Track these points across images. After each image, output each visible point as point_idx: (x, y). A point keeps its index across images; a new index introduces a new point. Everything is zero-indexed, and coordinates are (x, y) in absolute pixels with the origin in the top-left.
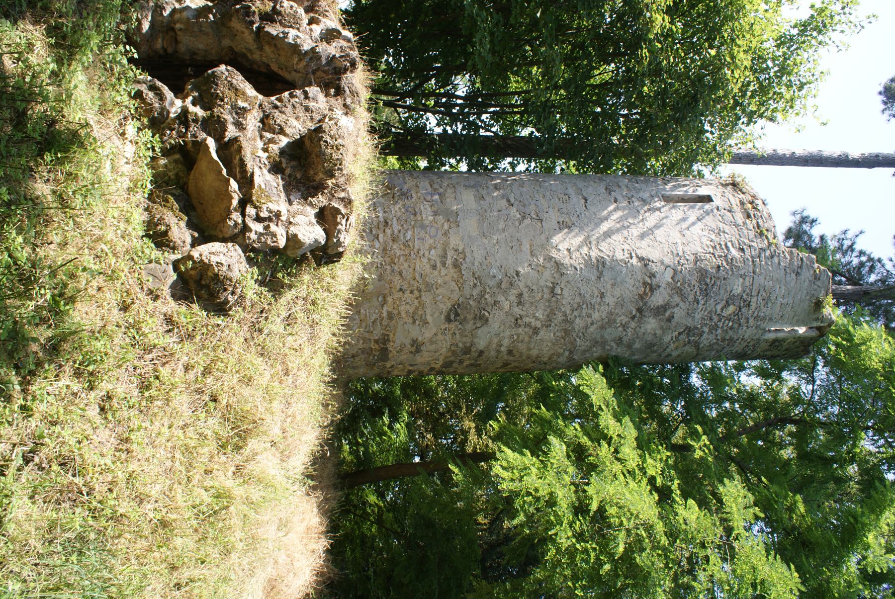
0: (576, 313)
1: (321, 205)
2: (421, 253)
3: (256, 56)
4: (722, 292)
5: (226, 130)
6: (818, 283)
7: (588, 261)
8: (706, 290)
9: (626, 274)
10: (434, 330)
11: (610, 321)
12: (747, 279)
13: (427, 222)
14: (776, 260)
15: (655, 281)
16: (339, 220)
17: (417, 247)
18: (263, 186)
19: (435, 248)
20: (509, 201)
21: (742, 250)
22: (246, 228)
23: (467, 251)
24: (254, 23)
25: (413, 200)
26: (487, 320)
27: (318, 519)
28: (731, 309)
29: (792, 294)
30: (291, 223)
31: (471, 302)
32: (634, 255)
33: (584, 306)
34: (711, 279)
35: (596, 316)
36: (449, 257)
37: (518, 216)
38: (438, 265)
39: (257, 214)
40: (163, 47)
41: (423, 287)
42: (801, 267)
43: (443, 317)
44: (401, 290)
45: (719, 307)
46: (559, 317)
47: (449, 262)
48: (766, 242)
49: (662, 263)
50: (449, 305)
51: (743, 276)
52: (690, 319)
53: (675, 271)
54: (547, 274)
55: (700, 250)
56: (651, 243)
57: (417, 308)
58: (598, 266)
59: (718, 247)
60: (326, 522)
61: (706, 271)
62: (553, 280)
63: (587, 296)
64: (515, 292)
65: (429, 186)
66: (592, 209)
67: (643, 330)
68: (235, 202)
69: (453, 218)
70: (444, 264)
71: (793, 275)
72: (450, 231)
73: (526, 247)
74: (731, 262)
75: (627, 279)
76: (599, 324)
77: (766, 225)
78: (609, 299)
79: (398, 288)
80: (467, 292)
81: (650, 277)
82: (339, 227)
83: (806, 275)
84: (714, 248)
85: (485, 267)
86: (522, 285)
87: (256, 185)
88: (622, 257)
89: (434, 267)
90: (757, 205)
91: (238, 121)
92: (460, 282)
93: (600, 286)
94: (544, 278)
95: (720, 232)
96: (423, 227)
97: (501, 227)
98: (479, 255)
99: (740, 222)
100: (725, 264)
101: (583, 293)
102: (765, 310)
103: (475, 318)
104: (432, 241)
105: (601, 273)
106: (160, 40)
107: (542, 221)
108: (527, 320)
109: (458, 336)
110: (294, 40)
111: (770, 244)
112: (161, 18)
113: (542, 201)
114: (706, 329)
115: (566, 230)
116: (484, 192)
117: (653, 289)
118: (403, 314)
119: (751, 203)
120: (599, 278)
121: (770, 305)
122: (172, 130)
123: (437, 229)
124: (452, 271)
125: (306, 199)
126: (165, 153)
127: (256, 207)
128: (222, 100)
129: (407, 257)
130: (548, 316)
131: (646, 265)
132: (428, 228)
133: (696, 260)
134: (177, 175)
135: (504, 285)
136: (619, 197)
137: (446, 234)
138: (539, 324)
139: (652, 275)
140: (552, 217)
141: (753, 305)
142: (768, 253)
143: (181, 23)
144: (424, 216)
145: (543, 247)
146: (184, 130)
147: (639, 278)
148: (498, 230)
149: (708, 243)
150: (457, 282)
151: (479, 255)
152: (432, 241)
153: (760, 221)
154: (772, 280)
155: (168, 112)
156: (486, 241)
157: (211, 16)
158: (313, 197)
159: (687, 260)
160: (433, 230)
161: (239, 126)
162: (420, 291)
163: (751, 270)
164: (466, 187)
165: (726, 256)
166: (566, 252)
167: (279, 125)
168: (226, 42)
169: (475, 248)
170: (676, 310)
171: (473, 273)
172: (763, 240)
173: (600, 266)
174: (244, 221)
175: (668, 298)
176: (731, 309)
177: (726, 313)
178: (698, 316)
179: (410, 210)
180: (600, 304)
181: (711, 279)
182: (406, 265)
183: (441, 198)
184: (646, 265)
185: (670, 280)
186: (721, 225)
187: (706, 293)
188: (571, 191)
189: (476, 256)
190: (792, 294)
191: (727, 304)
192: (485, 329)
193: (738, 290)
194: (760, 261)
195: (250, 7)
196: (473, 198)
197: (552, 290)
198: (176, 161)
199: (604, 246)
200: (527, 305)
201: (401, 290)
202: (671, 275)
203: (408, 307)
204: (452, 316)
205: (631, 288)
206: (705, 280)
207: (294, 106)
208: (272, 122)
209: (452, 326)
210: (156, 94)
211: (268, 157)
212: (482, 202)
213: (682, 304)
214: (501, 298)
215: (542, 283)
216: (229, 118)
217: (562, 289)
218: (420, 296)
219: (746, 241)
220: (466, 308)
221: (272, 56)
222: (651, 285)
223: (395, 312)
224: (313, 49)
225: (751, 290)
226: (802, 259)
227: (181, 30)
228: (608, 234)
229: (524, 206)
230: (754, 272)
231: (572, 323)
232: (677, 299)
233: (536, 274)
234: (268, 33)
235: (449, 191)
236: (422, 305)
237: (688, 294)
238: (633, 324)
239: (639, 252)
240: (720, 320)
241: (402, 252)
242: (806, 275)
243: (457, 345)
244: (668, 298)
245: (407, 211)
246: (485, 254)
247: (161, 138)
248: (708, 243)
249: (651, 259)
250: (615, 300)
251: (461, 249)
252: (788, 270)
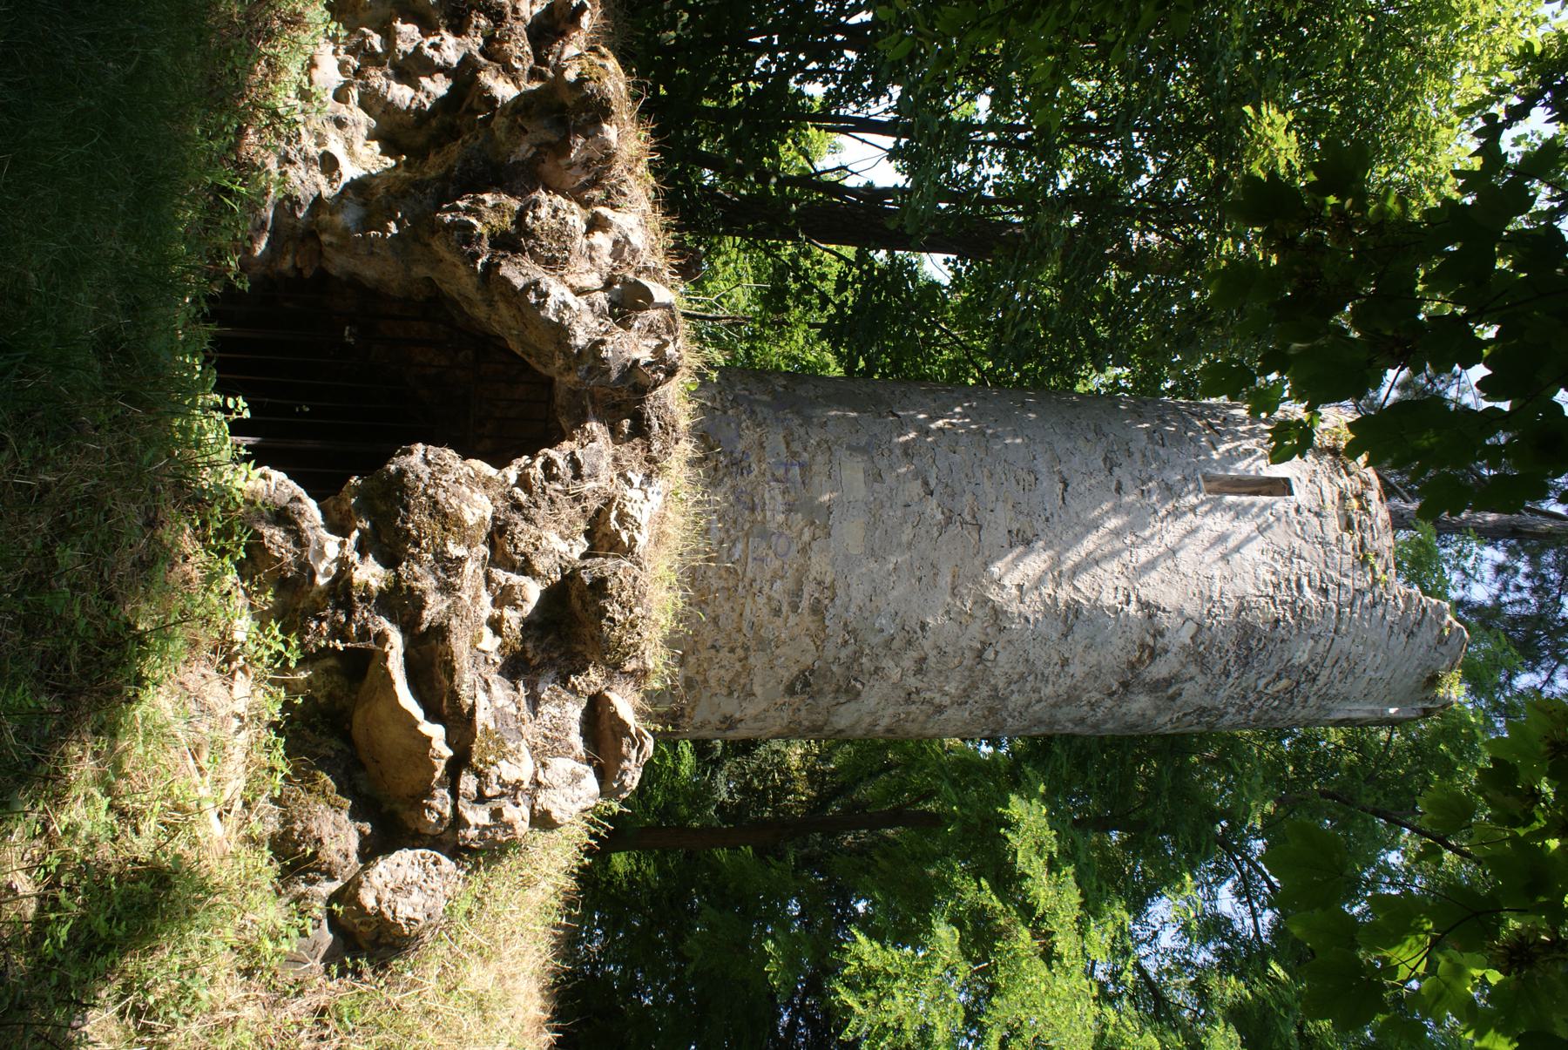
0: (1013, 687)
1: (593, 689)
2: (756, 586)
3: (481, 312)
4: (1273, 660)
5: (423, 608)
6: (1443, 650)
7: (1051, 609)
8: (1246, 657)
9: (1114, 632)
10: (764, 705)
11: (1071, 698)
12: (1322, 641)
13: (772, 526)
14: (1379, 610)
15: (1161, 642)
16: (624, 749)
17: (750, 575)
18: (492, 726)
19: (782, 578)
20: (926, 483)
21: (1325, 592)
22: (458, 821)
23: (840, 584)
24: (479, 257)
25: (752, 476)
26: (858, 694)
27: (539, 1002)
28: (1284, 683)
29: (1393, 666)
30: (539, 784)
31: (835, 668)
32: (1133, 598)
33: (1031, 678)
34: (1259, 640)
35: (1048, 690)
36: (806, 595)
37: (940, 517)
38: (785, 608)
39: (480, 790)
40: (294, 266)
41: (752, 644)
42: (1419, 624)
43: (781, 687)
44: (713, 647)
45: (1262, 683)
46: (985, 691)
47: (805, 604)
48: (1369, 578)
49: (1180, 612)
50: (795, 670)
51: (1316, 638)
52: (1208, 698)
53: (1200, 626)
54: (975, 629)
55: (1252, 591)
56: (1168, 576)
57: (738, 674)
58: (1066, 617)
59: (1283, 586)
60: (550, 1005)
61: (1254, 628)
62: (983, 638)
63: (1040, 664)
64: (915, 654)
65: (783, 446)
66: (1075, 505)
67: (1124, 710)
68: (441, 766)
69: (821, 519)
70: (795, 608)
71: (1403, 637)
72: (814, 545)
73: (945, 580)
74: (1300, 613)
75: (1114, 639)
76: (1051, 701)
77: (1376, 545)
78: (1076, 669)
79: (709, 644)
80: (830, 652)
81: (1154, 636)
82: (626, 764)
83: (1426, 636)
84: (1277, 586)
85: (867, 614)
86: (927, 644)
87: (479, 728)
88: (1112, 602)
89: (777, 612)
90: (1369, 502)
91: (446, 584)
92: (819, 638)
93: (1063, 648)
94: (968, 635)
95: (1293, 555)
96: (765, 535)
97: (905, 538)
98: (859, 593)
99: (1332, 537)
100: (1288, 615)
101: (1031, 657)
102: (1339, 686)
103: (837, 691)
104: (778, 563)
105: (1071, 628)
106: (289, 258)
107: (981, 527)
108: (928, 695)
109: (803, 713)
110: (558, 312)
111: (1375, 582)
112: (291, 221)
113: (987, 484)
114: (1232, 710)
115: (1021, 549)
116: (883, 464)
117: (1154, 654)
118: (713, 682)
119: (1358, 496)
120: (1065, 636)
121: (1350, 679)
122: (321, 619)
123: (790, 541)
124: (808, 620)
125: (564, 681)
126: (306, 660)
127: (479, 774)
128: (417, 544)
129: (730, 592)
130: (965, 690)
131: (1150, 617)
132: (774, 538)
133: (1241, 608)
134: (330, 696)
135: (896, 645)
136: (1127, 483)
137: (804, 551)
138: (946, 701)
139: (1159, 633)
140: (1001, 520)
141: (1322, 680)
142: (1368, 598)
143: (333, 234)
144: (768, 514)
145: (975, 579)
146: (343, 619)
147: (1135, 637)
148: (899, 545)
149: (1268, 577)
150: (814, 637)
151: (859, 593)
152: (778, 563)
153: (1368, 535)
154: (1364, 643)
155: (313, 574)
156: (873, 565)
157: (393, 227)
158: (578, 673)
159: (1225, 608)
160: (782, 541)
161: (446, 589)
162: (747, 649)
163: (1332, 627)
165: (1294, 602)
166: (1014, 591)
167: (523, 554)
168: (420, 271)
169: (854, 581)
170: (1187, 686)
171: (846, 624)
172: (1365, 574)
173: (1071, 617)
174: (455, 808)
175: (1177, 667)
176: (1284, 683)
177: (1270, 691)
178: (1222, 694)
179: (744, 498)
180: (1058, 675)
181: (1259, 640)
182: (727, 607)
183: (803, 475)
184: (1150, 617)
185: (1188, 641)
186: (1297, 543)
187: (1245, 662)
188: (1041, 465)
189: (854, 594)
190: (1393, 666)
191: (1279, 677)
192: (853, 706)
193: (1301, 657)
194: (1352, 612)
195: (473, 227)
196: (861, 475)
197: (980, 655)
198: (327, 671)
199: (1083, 582)
200: (931, 675)
201: (713, 647)
202: (1191, 633)
203: (722, 672)
204: (798, 687)
205: (1117, 652)
206: (1249, 640)
207: (552, 501)
208: (509, 549)
209: (797, 700)
210: (288, 531)
211: (502, 647)
212: (876, 485)
213: (1200, 678)
214: (887, 663)
215: (964, 643)
216: (428, 583)
217: (997, 653)
218: (746, 658)
219: (1335, 575)
220: (824, 676)
221: (512, 323)
222: (1153, 650)
223: (699, 678)
224: (596, 345)
225: (1324, 659)
226: (1424, 610)
227: (331, 244)
228: (1092, 561)
229: (953, 496)
230: (1336, 632)
231: (1005, 699)
232: (1193, 669)
233: (956, 628)
234: (506, 281)
235: (819, 458)
236: (749, 671)
237: (1215, 663)
238: (1109, 703)
239: (1143, 592)
240: (1259, 699)
241: (722, 584)
242: (1426, 636)
243: (800, 724)
244: (1177, 667)
245: (738, 499)
246: (870, 590)
247: (301, 639)
248: (1268, 577)
249: (1163, 605)
250: (1086, 669)
251: (828, 580)
252: (1396, 628)
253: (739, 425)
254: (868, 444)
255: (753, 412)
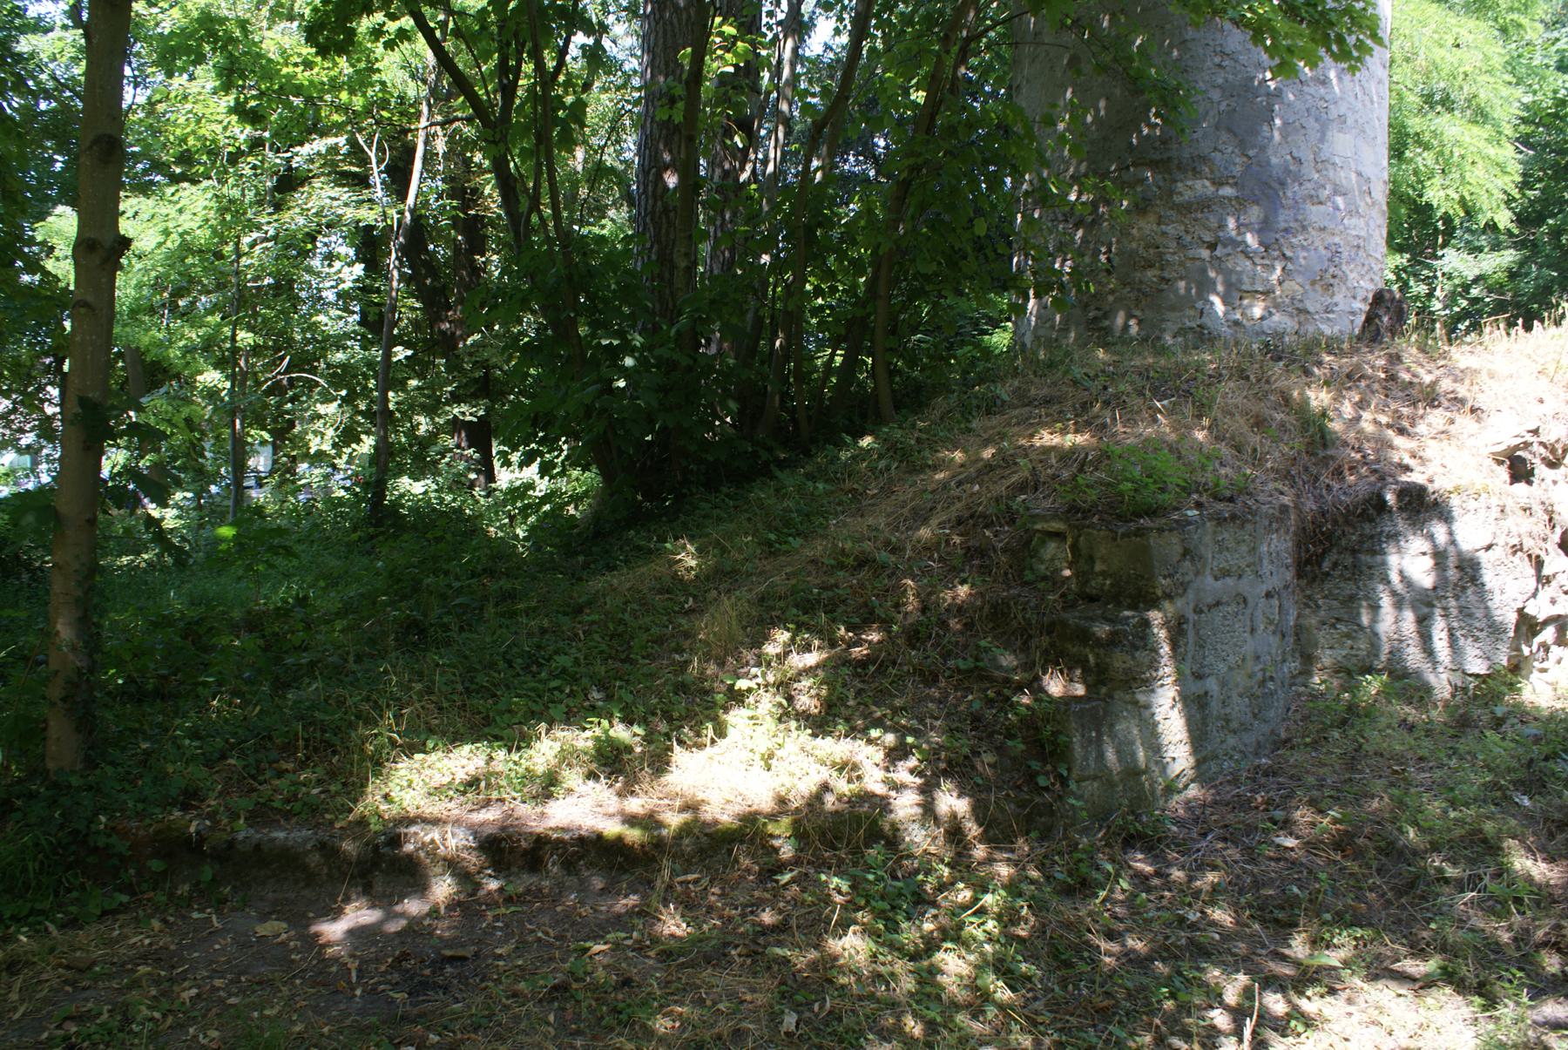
65: (1322, 208)
164: (1322, 140)
253: (1303, 248)
254: (1317, 120)
255: (1286, 230)
